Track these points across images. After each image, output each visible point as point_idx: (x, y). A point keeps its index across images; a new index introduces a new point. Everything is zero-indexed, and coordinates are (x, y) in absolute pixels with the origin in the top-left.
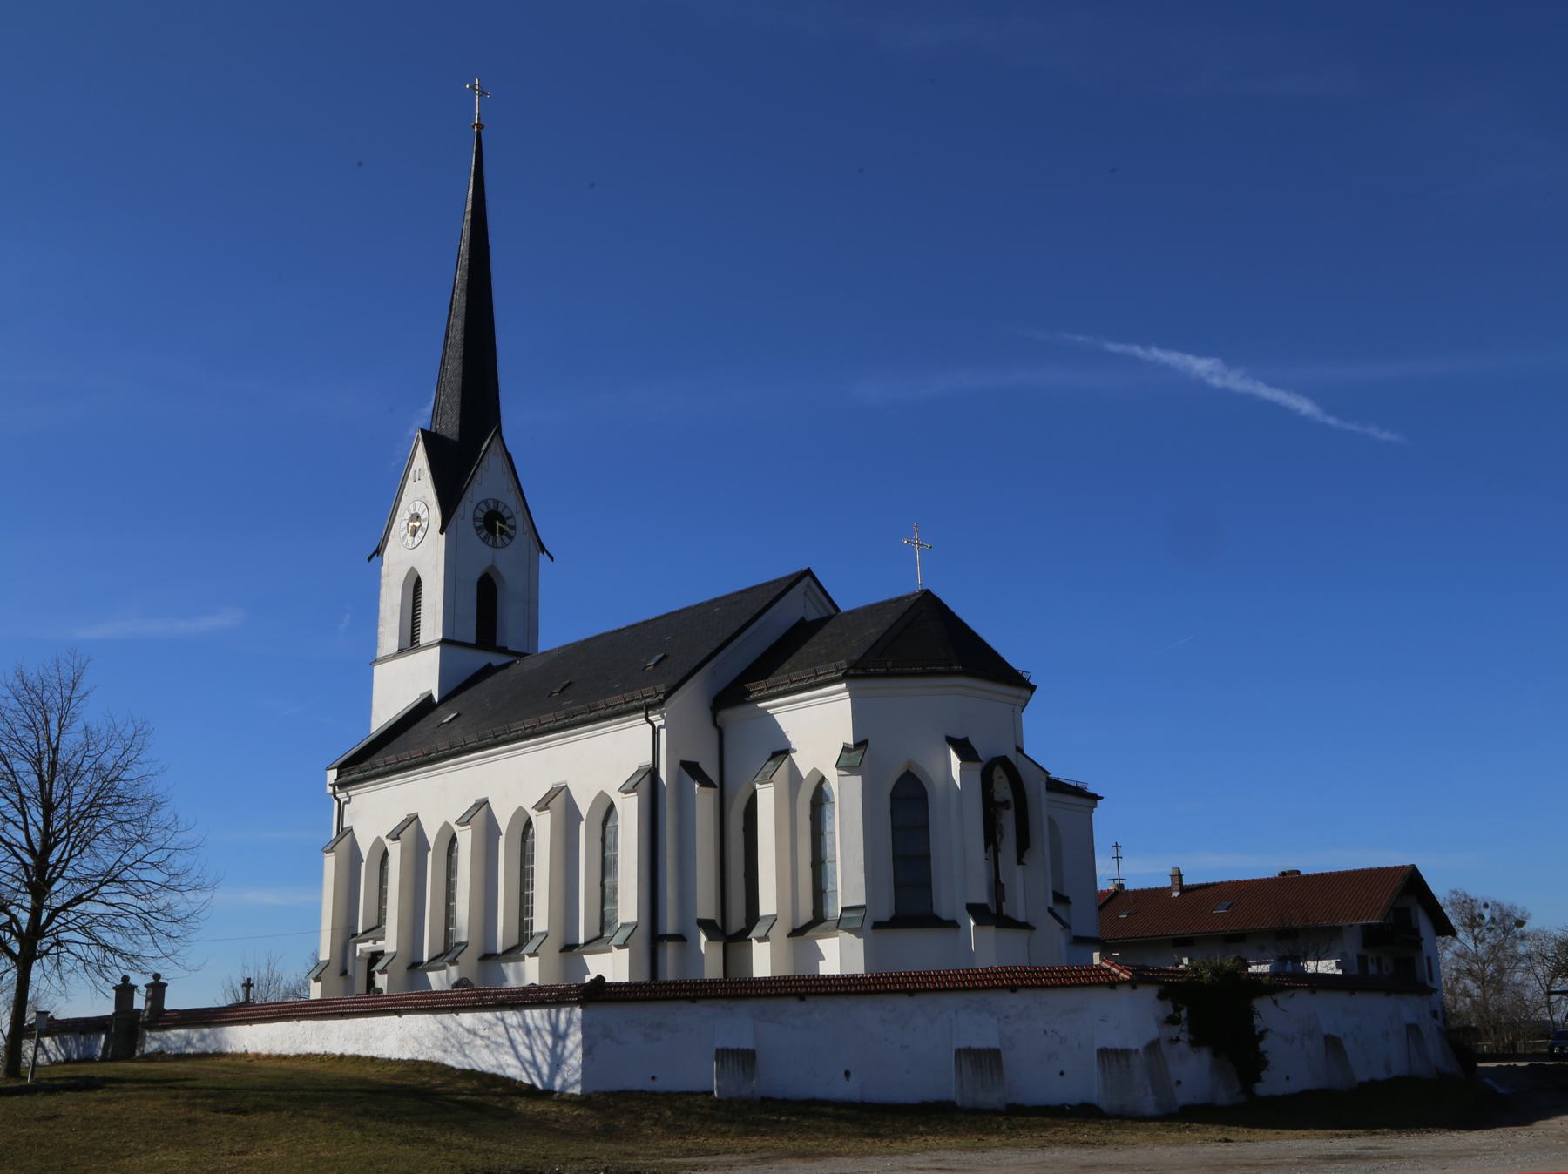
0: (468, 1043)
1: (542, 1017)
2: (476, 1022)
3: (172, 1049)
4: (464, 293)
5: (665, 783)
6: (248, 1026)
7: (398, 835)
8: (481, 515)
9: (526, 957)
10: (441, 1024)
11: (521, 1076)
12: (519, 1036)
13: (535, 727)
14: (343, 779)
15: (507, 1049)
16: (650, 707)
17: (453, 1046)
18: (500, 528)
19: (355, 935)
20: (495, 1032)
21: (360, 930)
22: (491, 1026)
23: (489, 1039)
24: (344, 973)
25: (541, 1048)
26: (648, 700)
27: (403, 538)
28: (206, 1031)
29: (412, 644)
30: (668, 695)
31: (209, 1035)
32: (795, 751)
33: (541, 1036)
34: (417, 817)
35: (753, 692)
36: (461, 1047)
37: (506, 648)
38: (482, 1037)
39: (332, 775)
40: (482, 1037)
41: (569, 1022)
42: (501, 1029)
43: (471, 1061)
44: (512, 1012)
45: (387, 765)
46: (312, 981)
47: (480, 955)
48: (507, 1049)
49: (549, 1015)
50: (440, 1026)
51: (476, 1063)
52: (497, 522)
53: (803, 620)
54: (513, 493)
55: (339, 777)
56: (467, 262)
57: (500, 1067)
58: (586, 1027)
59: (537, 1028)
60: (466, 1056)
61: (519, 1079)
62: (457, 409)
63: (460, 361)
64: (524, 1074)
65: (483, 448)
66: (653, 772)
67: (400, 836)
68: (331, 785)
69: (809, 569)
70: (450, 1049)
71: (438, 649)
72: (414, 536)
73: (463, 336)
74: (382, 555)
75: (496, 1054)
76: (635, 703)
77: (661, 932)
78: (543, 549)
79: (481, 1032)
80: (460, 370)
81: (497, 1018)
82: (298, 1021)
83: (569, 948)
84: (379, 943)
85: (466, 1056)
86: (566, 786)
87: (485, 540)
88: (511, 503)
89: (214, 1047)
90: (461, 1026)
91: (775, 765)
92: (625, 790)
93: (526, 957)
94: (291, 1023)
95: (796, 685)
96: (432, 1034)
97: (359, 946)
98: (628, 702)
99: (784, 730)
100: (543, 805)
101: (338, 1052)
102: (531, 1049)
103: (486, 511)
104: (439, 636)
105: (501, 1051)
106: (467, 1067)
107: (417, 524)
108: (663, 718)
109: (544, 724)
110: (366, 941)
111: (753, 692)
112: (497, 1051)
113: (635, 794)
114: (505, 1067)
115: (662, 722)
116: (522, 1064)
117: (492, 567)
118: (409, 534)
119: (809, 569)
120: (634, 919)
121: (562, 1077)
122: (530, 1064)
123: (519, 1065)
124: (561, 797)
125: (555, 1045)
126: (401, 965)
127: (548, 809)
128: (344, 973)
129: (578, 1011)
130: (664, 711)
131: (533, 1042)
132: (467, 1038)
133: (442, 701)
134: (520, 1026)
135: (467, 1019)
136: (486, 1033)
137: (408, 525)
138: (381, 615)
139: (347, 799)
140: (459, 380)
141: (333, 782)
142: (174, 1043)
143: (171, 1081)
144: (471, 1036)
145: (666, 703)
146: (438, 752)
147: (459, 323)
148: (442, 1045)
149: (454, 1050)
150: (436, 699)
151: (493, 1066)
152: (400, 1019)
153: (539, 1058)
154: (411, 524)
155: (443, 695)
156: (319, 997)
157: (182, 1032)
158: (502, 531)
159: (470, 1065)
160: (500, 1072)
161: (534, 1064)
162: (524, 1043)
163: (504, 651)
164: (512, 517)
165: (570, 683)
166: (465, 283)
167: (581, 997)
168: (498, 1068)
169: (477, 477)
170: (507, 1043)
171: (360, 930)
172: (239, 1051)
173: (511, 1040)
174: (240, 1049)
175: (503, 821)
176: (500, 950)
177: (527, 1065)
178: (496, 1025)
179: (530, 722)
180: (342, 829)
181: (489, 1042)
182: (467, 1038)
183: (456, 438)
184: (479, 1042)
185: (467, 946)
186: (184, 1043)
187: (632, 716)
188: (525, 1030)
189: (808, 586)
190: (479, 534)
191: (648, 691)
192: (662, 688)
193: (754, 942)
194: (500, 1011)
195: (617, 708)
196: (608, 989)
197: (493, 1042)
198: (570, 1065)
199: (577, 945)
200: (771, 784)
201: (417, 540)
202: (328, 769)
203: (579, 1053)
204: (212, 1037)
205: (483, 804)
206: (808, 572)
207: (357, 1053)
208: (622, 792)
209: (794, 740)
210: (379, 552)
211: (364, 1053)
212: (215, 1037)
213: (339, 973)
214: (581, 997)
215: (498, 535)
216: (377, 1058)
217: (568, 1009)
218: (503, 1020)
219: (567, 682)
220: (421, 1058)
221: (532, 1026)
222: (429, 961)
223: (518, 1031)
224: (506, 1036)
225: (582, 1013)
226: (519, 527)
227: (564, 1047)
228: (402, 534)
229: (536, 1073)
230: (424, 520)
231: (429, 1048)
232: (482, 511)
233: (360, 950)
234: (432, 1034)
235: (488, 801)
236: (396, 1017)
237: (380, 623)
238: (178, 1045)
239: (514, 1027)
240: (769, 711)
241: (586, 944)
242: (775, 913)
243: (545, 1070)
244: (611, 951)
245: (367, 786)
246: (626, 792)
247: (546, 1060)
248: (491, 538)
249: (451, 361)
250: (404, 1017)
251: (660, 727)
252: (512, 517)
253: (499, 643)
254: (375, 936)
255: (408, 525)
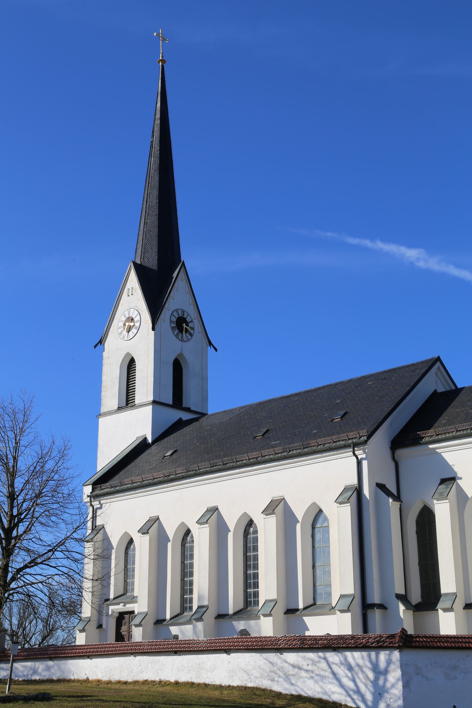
0: (294, 675)
1: (363, 657)
2: (300, 659)
3: (19, 676)
4: (157, 172)
5: (368, 498)
6: (89, 660)
7: (148, 530)
8: (174, 319)
9: (262, 617)
10: (267, 660)
11: (346, 701)
12: (341, 672)
13: (257, 458)
14: (97, 492)
15: (330, 680)
16: (355, 445)
17: (279, 677)
18: (186, 328)
19: (108, 600)
20: (318, 668)
21: (112, 597)
22: (314, 663)
23: (312, 672)
24: (100, 626)
25: (364, 680)
26: (354, 441)
27: (121, 333)
28: (50, 663)
29: (127, 404)
30: (369, 437)
31: (53, 667)
32: (461, 478)
33: (363, 671)
34: (158, 518)
35: (423, 437)
36: (287, 678)
37: (190, 408)
38: (307, 671)
39: (88, 490)
40: (307, 671)
41: (389, 662)
42: (324, 665)
43: (297, 688)
44: (335, 653)
45: (276, 454)
46: (78, 632)
47: (216, 615)
48: (330, 680)
49: (369, 656)
50: (266, 662)
51: (302, 690)
52: (184, 324)
53: (435, 392)
54: (192, 305)
55: (93, 489)
56: (159, 152)
57: (325, 693)
58: (403, 666)
59: (358, 665)
60: (292, 684)
61: (343, 703)
62: (155, 249)
63: (156, 217)
64: (349, 699)
65: (175, 275)
66: (359, 490)
67: (149, 531)
68: (88, 496)
69: (439, 357)
70: (276, 679)
71: (151, 407)
72: (129, 332)
73: (158, 201)
74: (104, 345)
75: (320, 683)
76: (342, 443)
77: (369, 601)
78: (210, 343)
79: (305, 667)
80: (156, 223)
81: (320, 657)
82: (135, 656)
83: (291, 611)
84: (128, 606)
85: (292, 684)
86: (284, 498)
87: (176, 336)
88: (191, 314)
89: (58, 675)
90: (286, 662)
91: (447, 488)
92: (339, 501)
93: (262, 617)
94: (128, 658)
95: (461, 433)
96: (259, 667)
97: (111, 608)
98: (336, 442)
99: (451, 464)
100: (144, 531)
101: (172, 680)
102: (354, 681)
103: (177, 317)
104: (151, 399)
105: (325, 681)
106: (294, 693)
107: (132, 324)
108: (365, 452)
109: (264, 456)
110: (118, 604)
111: (423, 437)
112: (322, 681)
113: (349, 504)
114: (330, 693)
115: (364, 456)
116: (346, 691)
117: (181, 355)
118: (125, 331)
119: (439, 357)
120: (352, 592)
121: (386, 702)
122: (354, 692)
123: (344, 692)
124: (281, 505)
125: (377, 679)
126: (151, 620)
127: (274, 513)
128: (100, 626)
129: (396, 654)
130: (366, 448)
131: (356, 676)
132: (292, 671)
133: (154, 442)
134: (342, 663)
135: (291, 657)
136: (310, 668)
137: (125, 325)
138: (104, 384)
139: (99, 506)
140: (156, 230)
141: (89, 494)
142: (22, 672)
143: (88, 696)
144: (296, 670)
145: (368, 443)
146: (176, 475)
147: (155, 193)
148: (268, 676)
149: (281, 680)
150: (150, 440)
151: (319, 693)
152: (91, 660)
153: (363, 688)
154: (127, 324)
155: (155, 438)
156: (84, 643)
157: (29, 664)
158: (187, 331)
159: (296, 691)
160: (325, 697)
161: (358, 692)
162: (347, 676)
163: (188, 410)
164: (191, 322)
165: (268, 431)
166: (157, 166)
167: (401, 644)
168: (323, 694)
169: (172, 294)
170: (331, 676)
171: (112, 597)
172: (81, 678)
173: (334, 674)
174: (83, 677)
175: (231, 522)
176: (231, 612)
177: (351, 693)
178: (319, 662)
179: (254, 454)
180: (96, 527)
181: (313, 675)
182: (292, 671)
183: (155, 267)
184: (303, 674)
185: (208, 608)
186: (31, 672)
187: (339, 452)
188: (346, 667)
189: (439, 368)
190: (173, 332)
191: (351, 435)
192: (364, 432)
193: (440, 612)
194: (323, 652)
195: (327, 445)
196: (414, 640)
197: (317, 675)
198: (392, 694)
199: (298, 610)
200: (447, 501)
201: (131, 334)
202: (84, 485)
203: (400, 685)
204: (56, 668)
205: (215, 510)
206: (438, 359)
207: (190, 681)
208: (337, 503)
209: (459, 470)
210: (101, 342)
211: (196, 681)
212: (59, 668)
213: (96, 626)
214: (401, 644)
215: (184, 333)
216: (209, 685)
217: (387, 652)
218: (325, 659)
219: (265, 430)
220: (250, 685)
221: (353, 663)
222: (171, 619)
223: (340, 667)
224: (329, 670)
225: (400, 655)
226: (196, 329)
227: (386, 680)
228: (120, 331)
229: (360, 699)
230: (137, 322)
231: (257, 677)
232: (174, 316)
233: (112, 610)
234: (259, 667)
235: (218, 508)
236: (225, 655)
237: (103, 389)
238: (25, 673)
239: (336, 664)
240: (437, 450)
241: (305, 609)
242: (455, 591)
243: (369, 697)
244: (335, 614)
245: (107, 499)
246: (341, 503)
247: (369, 689)
248: (180, 334)
249: (150, 217)
250: (232, 655)
251: (362, 459)
252: (191, 322)
253: (184, 405)
254: (126, 600)
255: (125, 325)
